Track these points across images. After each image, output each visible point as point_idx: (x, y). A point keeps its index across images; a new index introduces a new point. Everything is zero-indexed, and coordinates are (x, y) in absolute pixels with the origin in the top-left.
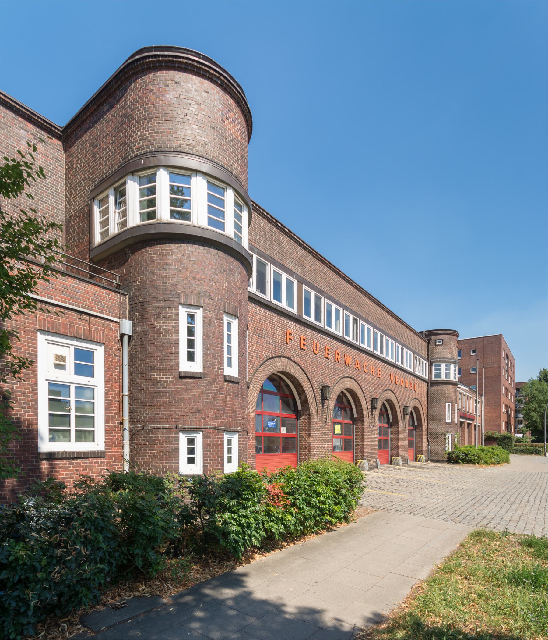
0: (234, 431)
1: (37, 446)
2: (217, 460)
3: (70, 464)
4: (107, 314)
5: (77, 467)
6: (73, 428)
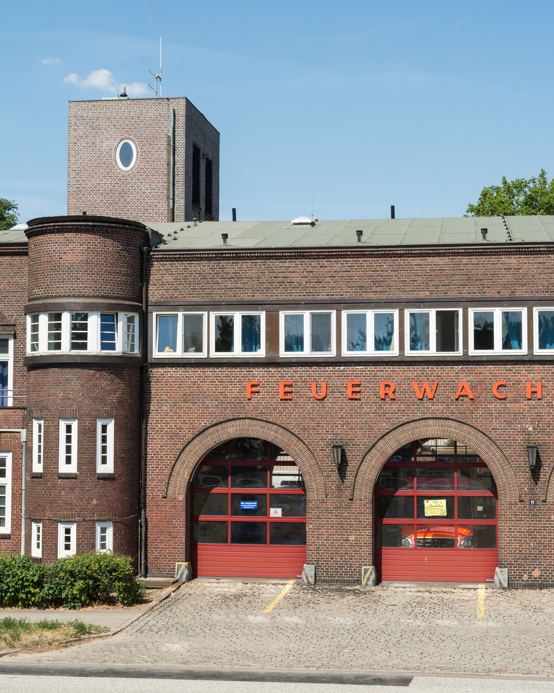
0: (72, 522)
2: (51, 546)
4: (13, 428)
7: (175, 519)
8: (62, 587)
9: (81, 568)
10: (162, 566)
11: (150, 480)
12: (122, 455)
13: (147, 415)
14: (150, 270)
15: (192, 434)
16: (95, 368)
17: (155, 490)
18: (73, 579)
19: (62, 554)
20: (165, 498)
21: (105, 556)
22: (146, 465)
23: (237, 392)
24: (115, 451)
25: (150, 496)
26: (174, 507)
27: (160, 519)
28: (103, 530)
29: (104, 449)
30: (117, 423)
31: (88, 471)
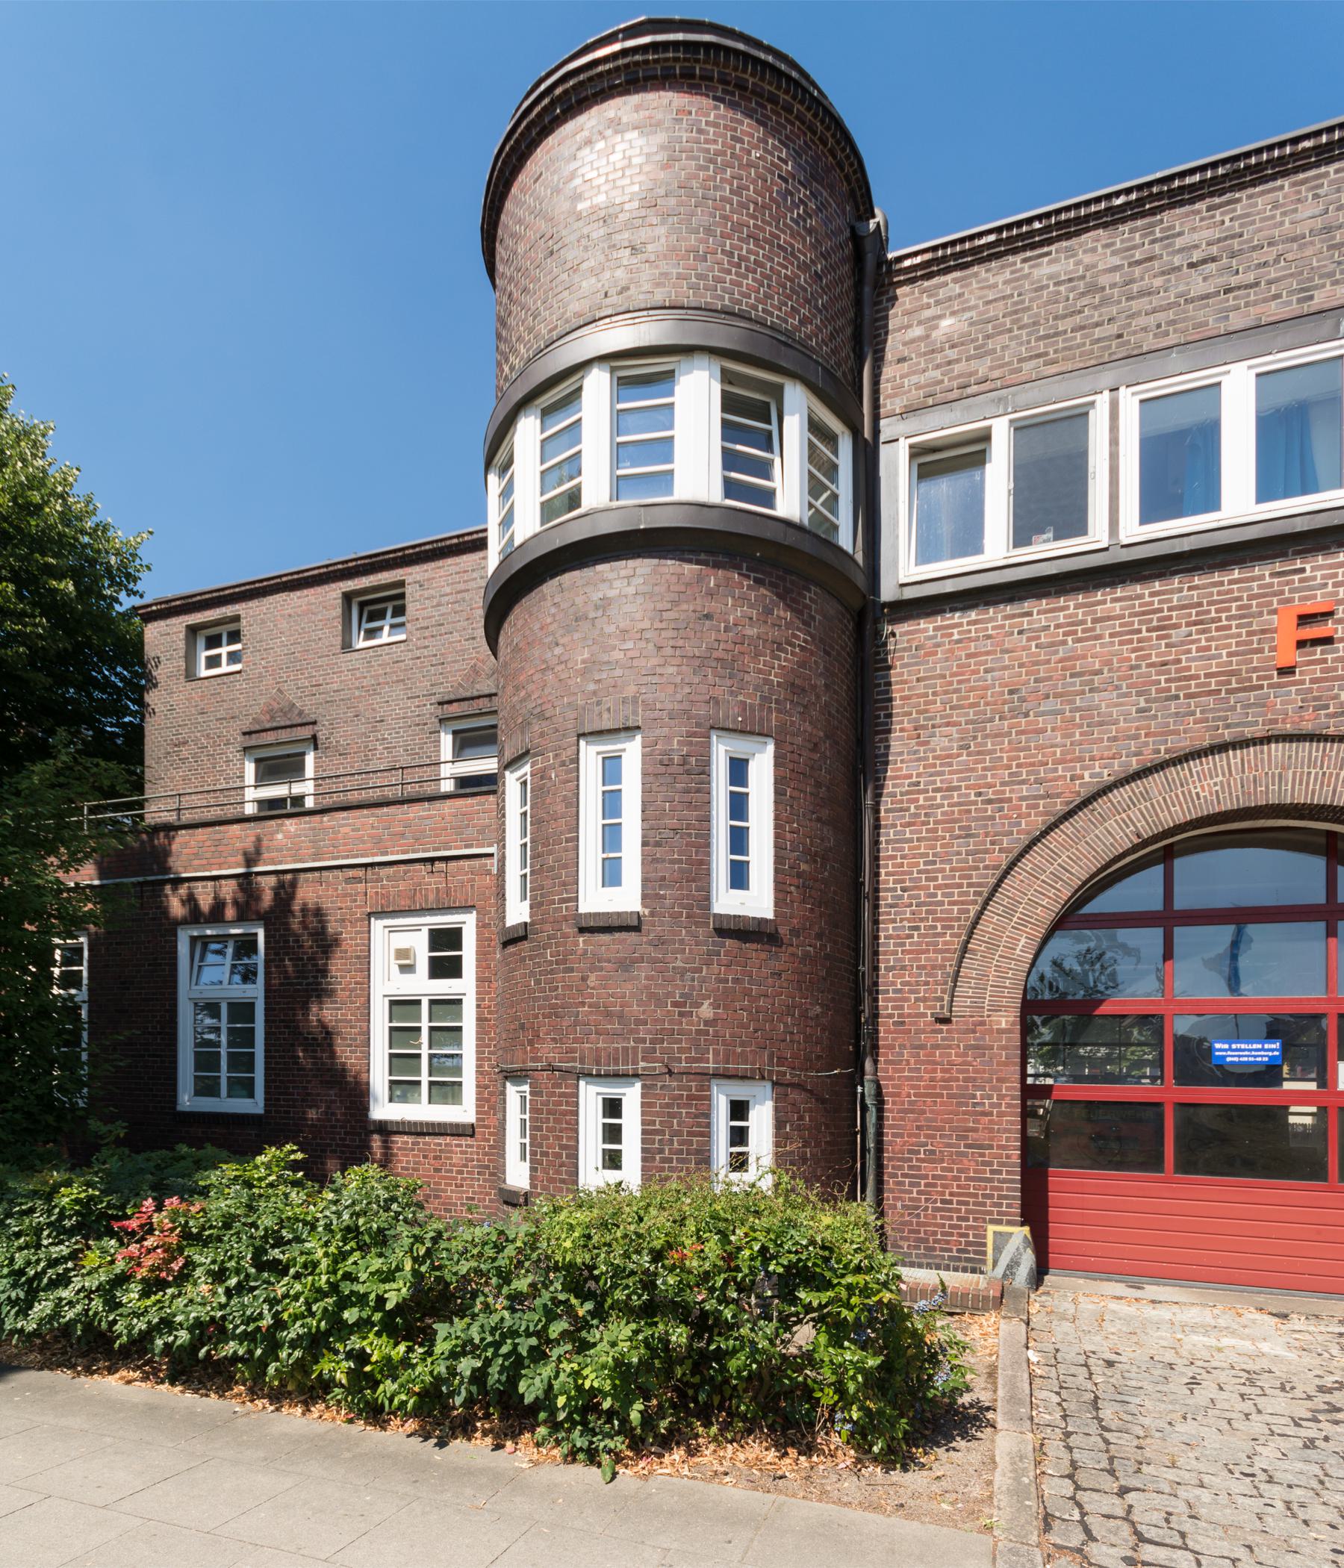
0: (626, 1075)
1: (368, 1109)
2: (558, 1155)
3: (413, 1144)
5: (425, 1150)
6: (425, 1078)
7: (983, 1089)
8: (525, 1345)
9: (626, 1256)
10: (935, 1233)
11: (888, 969)
12: (803, 867)
13: (877, 771)
14: (886, 317)
15: (1046, 813)
16: (703, 557)
17: (907, 1000)
18: (589, 1306)
19: (592, 1176)
20: (946, 1021)
21: (751, 1205)
22: (876, 922)
23: (1230, 655)
24: (778, 847)
25: (891, 1016)
26: (979, 1049)
27: (926, 1087)
28: (739, 1110)
29: (739, 840)
30: (784, 756)
31: (681, 906)
